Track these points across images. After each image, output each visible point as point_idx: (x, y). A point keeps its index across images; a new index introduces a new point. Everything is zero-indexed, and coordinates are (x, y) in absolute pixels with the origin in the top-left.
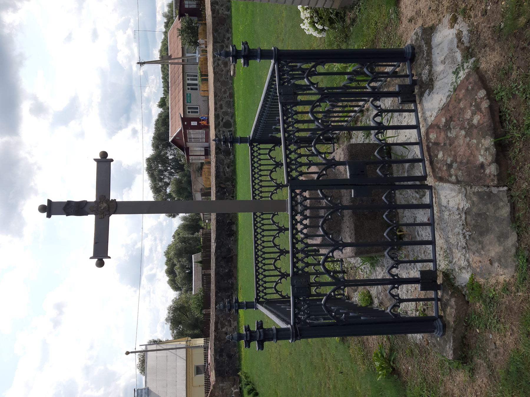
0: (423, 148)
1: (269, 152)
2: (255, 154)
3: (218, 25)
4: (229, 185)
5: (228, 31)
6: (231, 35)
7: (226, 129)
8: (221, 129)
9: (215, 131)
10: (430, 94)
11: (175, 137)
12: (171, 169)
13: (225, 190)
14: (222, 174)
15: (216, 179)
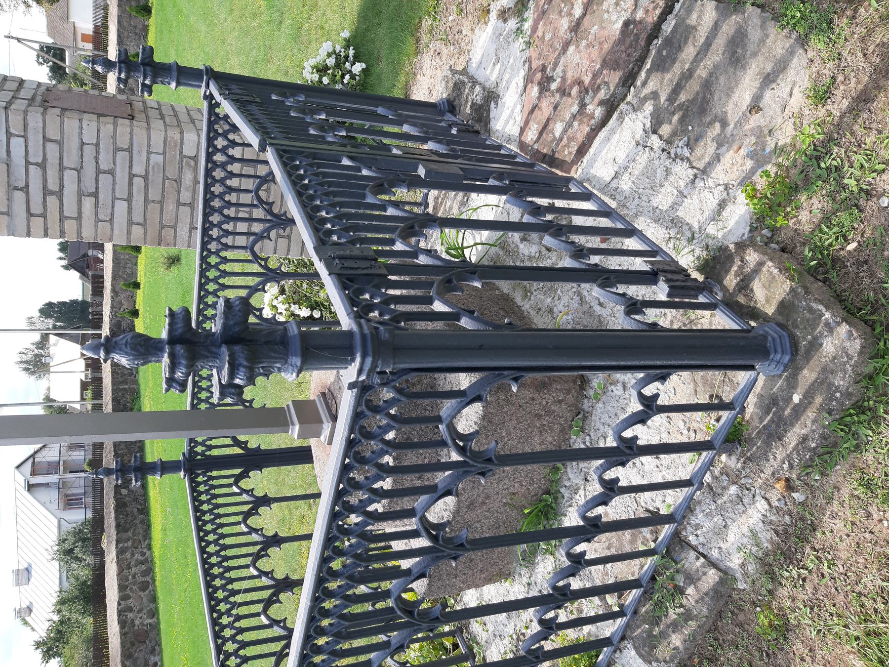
1: (255, 242)
2: (213, 246)
3: (134, 645)
5: (153, 652)
6: (159, 657)
10: (497, 105)
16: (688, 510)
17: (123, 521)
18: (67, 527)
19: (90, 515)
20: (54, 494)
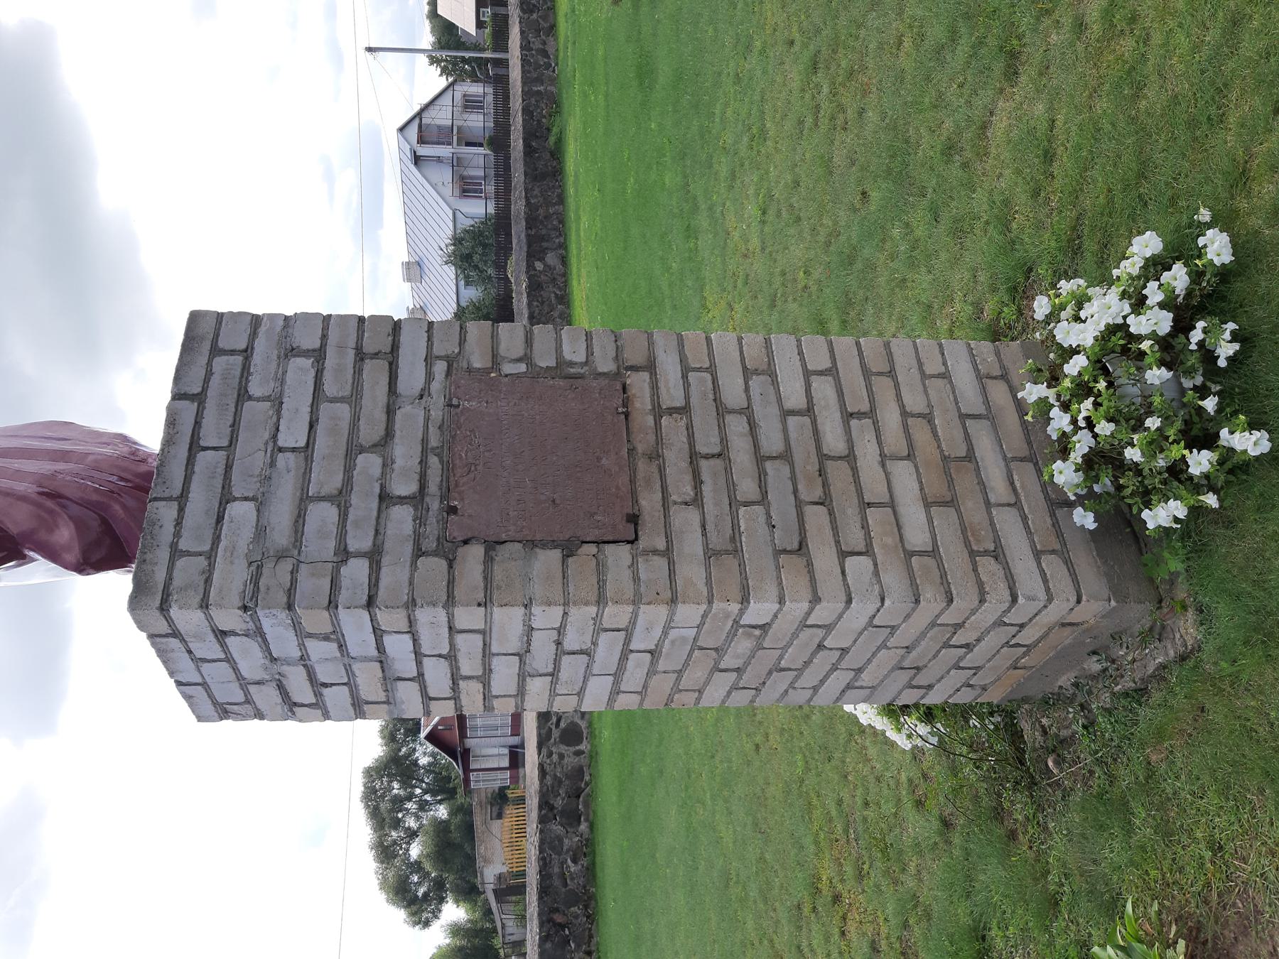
0: (441, 197)
4: (576, 917)
7: (567, 748)
8: (554, 750)
9: (539, 754)
11: (435, 726)
12: (425, 792)
13: (567, 932)
14: (557, 882)
15: (540, 898)
16: (1060, 513)
17: (537, 311)
18: (465, 223)
19: (491, 210)
20: (446, 175)
